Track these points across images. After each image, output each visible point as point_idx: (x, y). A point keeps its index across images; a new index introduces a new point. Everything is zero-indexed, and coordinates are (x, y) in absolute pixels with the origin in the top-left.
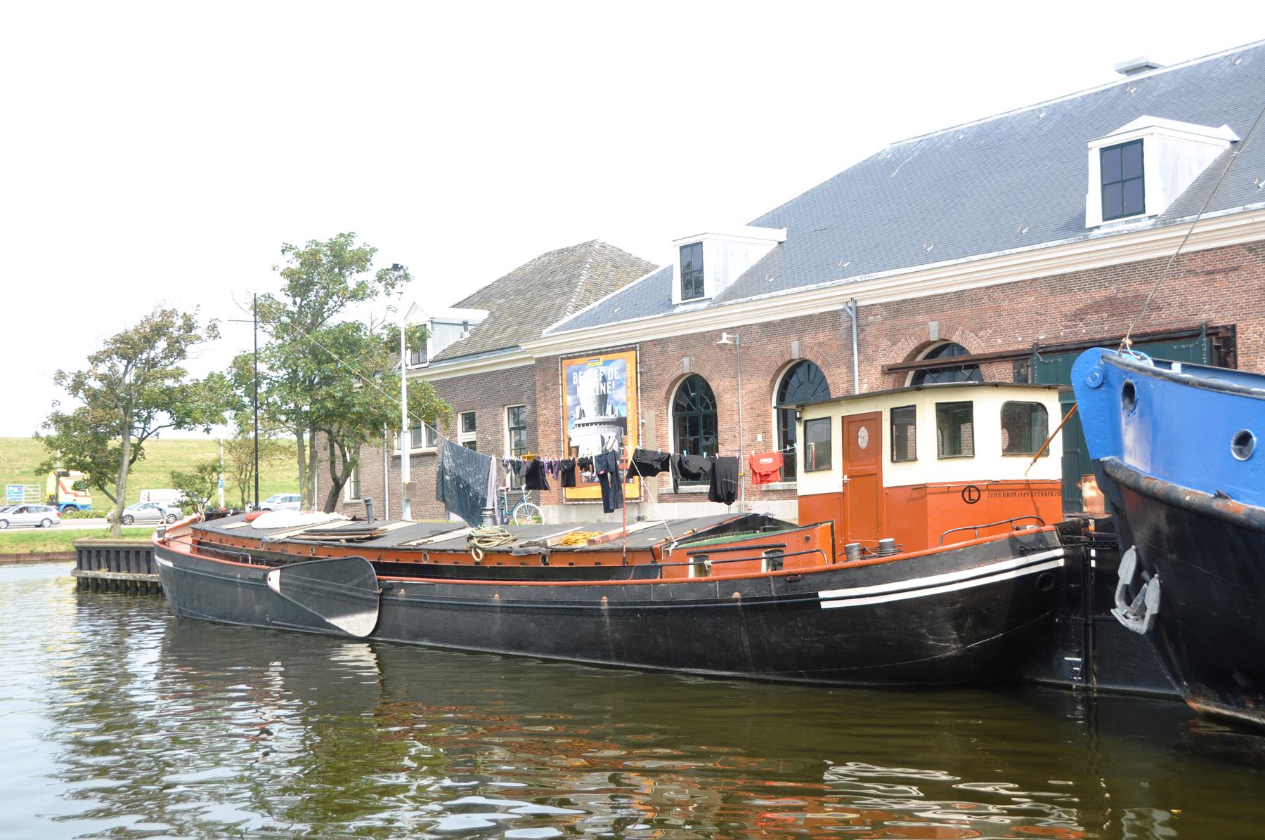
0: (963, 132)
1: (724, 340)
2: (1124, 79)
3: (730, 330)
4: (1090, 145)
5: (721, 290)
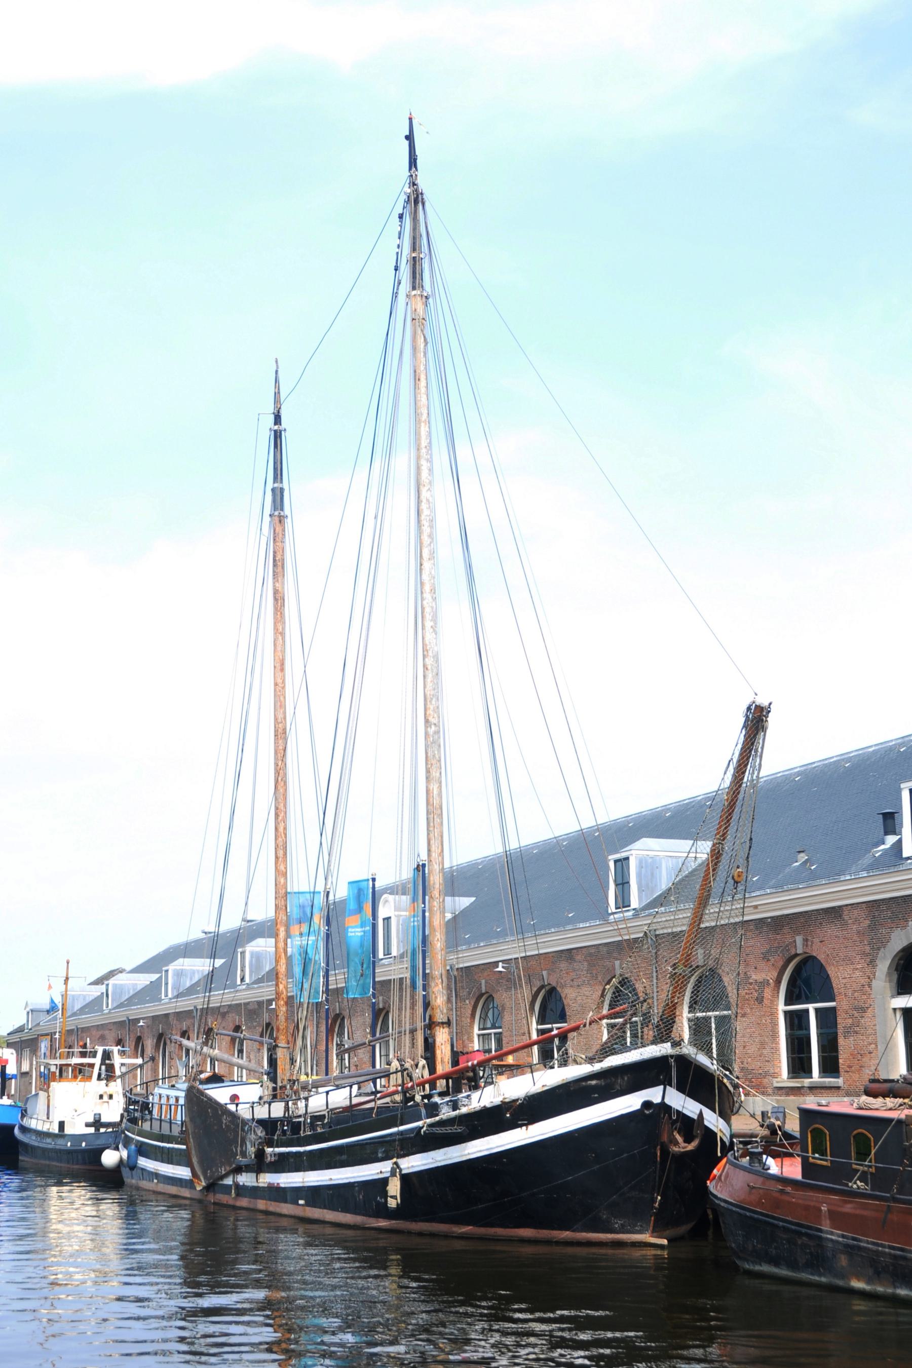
0: (798, 774)
1: (141, 1024)
2: (203, 936)
3: (143, 1019)
4: (902, 786)
5: (254, 979)
